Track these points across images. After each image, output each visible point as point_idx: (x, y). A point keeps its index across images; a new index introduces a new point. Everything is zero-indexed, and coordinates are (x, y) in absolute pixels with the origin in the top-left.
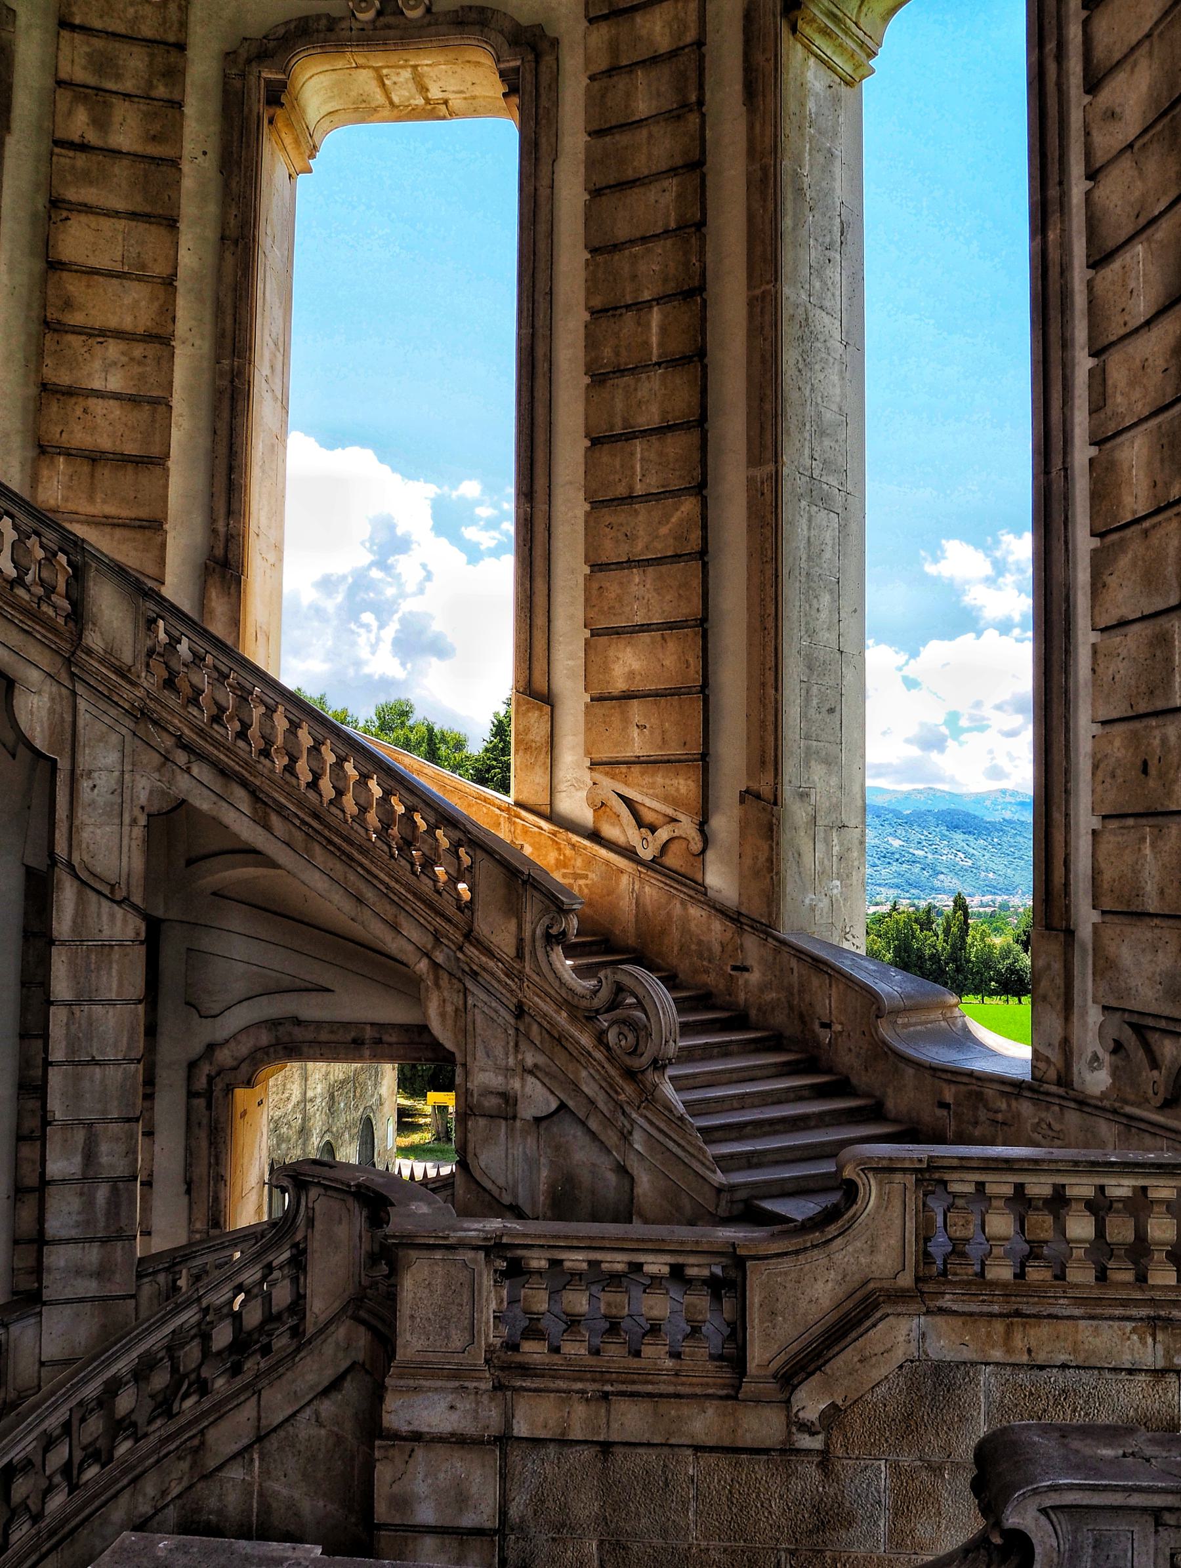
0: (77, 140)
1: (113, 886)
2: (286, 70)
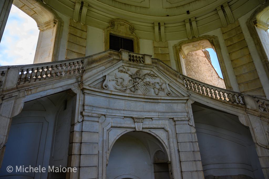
0: (230, 45)
1: (266, 146)
2: (256, 18)
